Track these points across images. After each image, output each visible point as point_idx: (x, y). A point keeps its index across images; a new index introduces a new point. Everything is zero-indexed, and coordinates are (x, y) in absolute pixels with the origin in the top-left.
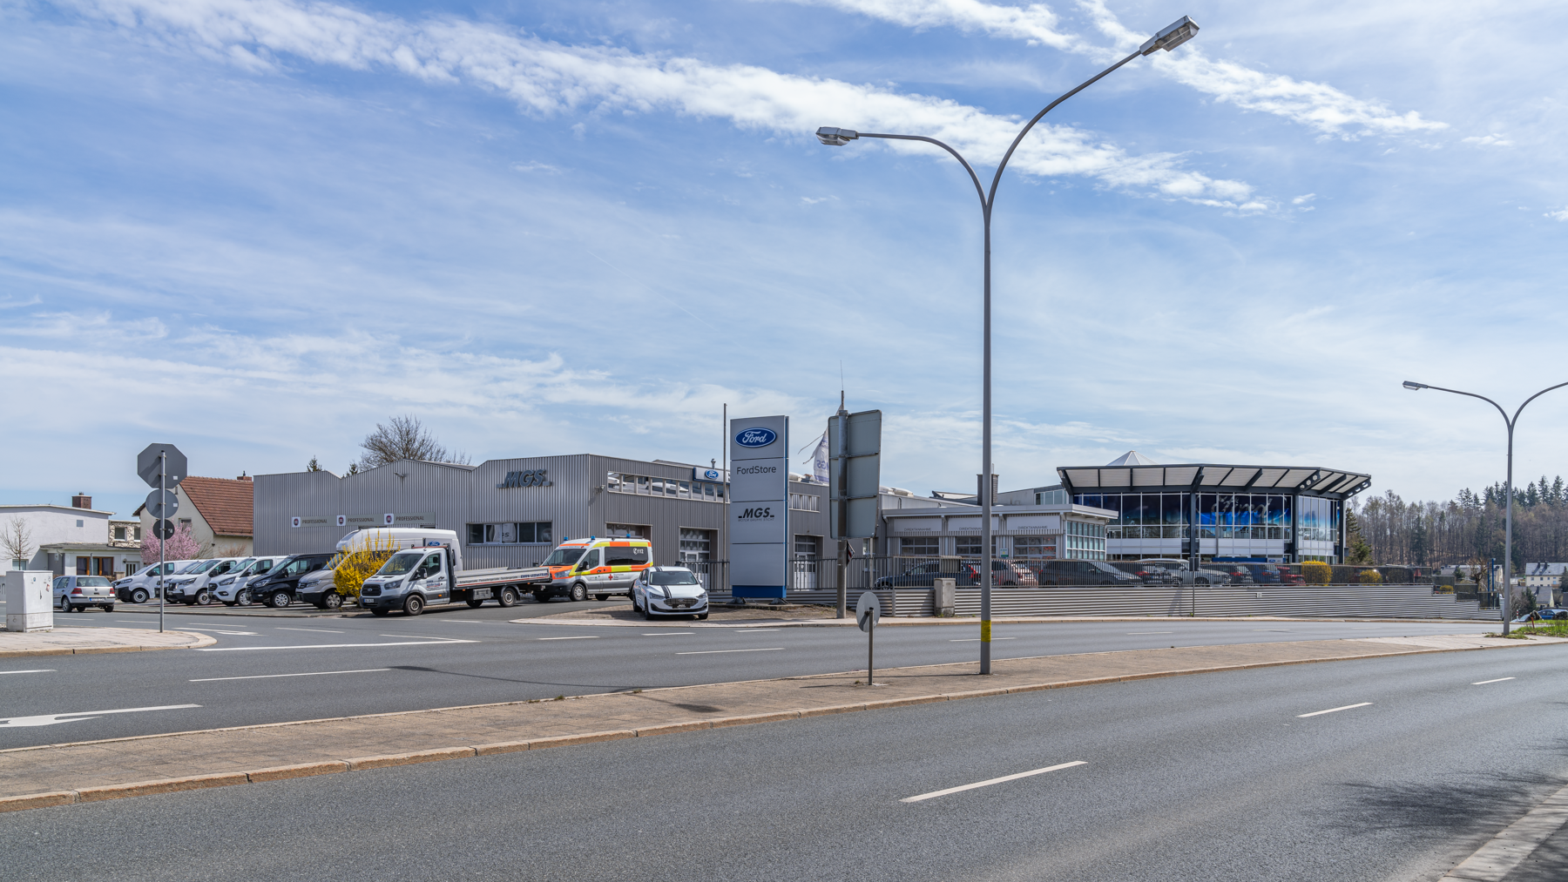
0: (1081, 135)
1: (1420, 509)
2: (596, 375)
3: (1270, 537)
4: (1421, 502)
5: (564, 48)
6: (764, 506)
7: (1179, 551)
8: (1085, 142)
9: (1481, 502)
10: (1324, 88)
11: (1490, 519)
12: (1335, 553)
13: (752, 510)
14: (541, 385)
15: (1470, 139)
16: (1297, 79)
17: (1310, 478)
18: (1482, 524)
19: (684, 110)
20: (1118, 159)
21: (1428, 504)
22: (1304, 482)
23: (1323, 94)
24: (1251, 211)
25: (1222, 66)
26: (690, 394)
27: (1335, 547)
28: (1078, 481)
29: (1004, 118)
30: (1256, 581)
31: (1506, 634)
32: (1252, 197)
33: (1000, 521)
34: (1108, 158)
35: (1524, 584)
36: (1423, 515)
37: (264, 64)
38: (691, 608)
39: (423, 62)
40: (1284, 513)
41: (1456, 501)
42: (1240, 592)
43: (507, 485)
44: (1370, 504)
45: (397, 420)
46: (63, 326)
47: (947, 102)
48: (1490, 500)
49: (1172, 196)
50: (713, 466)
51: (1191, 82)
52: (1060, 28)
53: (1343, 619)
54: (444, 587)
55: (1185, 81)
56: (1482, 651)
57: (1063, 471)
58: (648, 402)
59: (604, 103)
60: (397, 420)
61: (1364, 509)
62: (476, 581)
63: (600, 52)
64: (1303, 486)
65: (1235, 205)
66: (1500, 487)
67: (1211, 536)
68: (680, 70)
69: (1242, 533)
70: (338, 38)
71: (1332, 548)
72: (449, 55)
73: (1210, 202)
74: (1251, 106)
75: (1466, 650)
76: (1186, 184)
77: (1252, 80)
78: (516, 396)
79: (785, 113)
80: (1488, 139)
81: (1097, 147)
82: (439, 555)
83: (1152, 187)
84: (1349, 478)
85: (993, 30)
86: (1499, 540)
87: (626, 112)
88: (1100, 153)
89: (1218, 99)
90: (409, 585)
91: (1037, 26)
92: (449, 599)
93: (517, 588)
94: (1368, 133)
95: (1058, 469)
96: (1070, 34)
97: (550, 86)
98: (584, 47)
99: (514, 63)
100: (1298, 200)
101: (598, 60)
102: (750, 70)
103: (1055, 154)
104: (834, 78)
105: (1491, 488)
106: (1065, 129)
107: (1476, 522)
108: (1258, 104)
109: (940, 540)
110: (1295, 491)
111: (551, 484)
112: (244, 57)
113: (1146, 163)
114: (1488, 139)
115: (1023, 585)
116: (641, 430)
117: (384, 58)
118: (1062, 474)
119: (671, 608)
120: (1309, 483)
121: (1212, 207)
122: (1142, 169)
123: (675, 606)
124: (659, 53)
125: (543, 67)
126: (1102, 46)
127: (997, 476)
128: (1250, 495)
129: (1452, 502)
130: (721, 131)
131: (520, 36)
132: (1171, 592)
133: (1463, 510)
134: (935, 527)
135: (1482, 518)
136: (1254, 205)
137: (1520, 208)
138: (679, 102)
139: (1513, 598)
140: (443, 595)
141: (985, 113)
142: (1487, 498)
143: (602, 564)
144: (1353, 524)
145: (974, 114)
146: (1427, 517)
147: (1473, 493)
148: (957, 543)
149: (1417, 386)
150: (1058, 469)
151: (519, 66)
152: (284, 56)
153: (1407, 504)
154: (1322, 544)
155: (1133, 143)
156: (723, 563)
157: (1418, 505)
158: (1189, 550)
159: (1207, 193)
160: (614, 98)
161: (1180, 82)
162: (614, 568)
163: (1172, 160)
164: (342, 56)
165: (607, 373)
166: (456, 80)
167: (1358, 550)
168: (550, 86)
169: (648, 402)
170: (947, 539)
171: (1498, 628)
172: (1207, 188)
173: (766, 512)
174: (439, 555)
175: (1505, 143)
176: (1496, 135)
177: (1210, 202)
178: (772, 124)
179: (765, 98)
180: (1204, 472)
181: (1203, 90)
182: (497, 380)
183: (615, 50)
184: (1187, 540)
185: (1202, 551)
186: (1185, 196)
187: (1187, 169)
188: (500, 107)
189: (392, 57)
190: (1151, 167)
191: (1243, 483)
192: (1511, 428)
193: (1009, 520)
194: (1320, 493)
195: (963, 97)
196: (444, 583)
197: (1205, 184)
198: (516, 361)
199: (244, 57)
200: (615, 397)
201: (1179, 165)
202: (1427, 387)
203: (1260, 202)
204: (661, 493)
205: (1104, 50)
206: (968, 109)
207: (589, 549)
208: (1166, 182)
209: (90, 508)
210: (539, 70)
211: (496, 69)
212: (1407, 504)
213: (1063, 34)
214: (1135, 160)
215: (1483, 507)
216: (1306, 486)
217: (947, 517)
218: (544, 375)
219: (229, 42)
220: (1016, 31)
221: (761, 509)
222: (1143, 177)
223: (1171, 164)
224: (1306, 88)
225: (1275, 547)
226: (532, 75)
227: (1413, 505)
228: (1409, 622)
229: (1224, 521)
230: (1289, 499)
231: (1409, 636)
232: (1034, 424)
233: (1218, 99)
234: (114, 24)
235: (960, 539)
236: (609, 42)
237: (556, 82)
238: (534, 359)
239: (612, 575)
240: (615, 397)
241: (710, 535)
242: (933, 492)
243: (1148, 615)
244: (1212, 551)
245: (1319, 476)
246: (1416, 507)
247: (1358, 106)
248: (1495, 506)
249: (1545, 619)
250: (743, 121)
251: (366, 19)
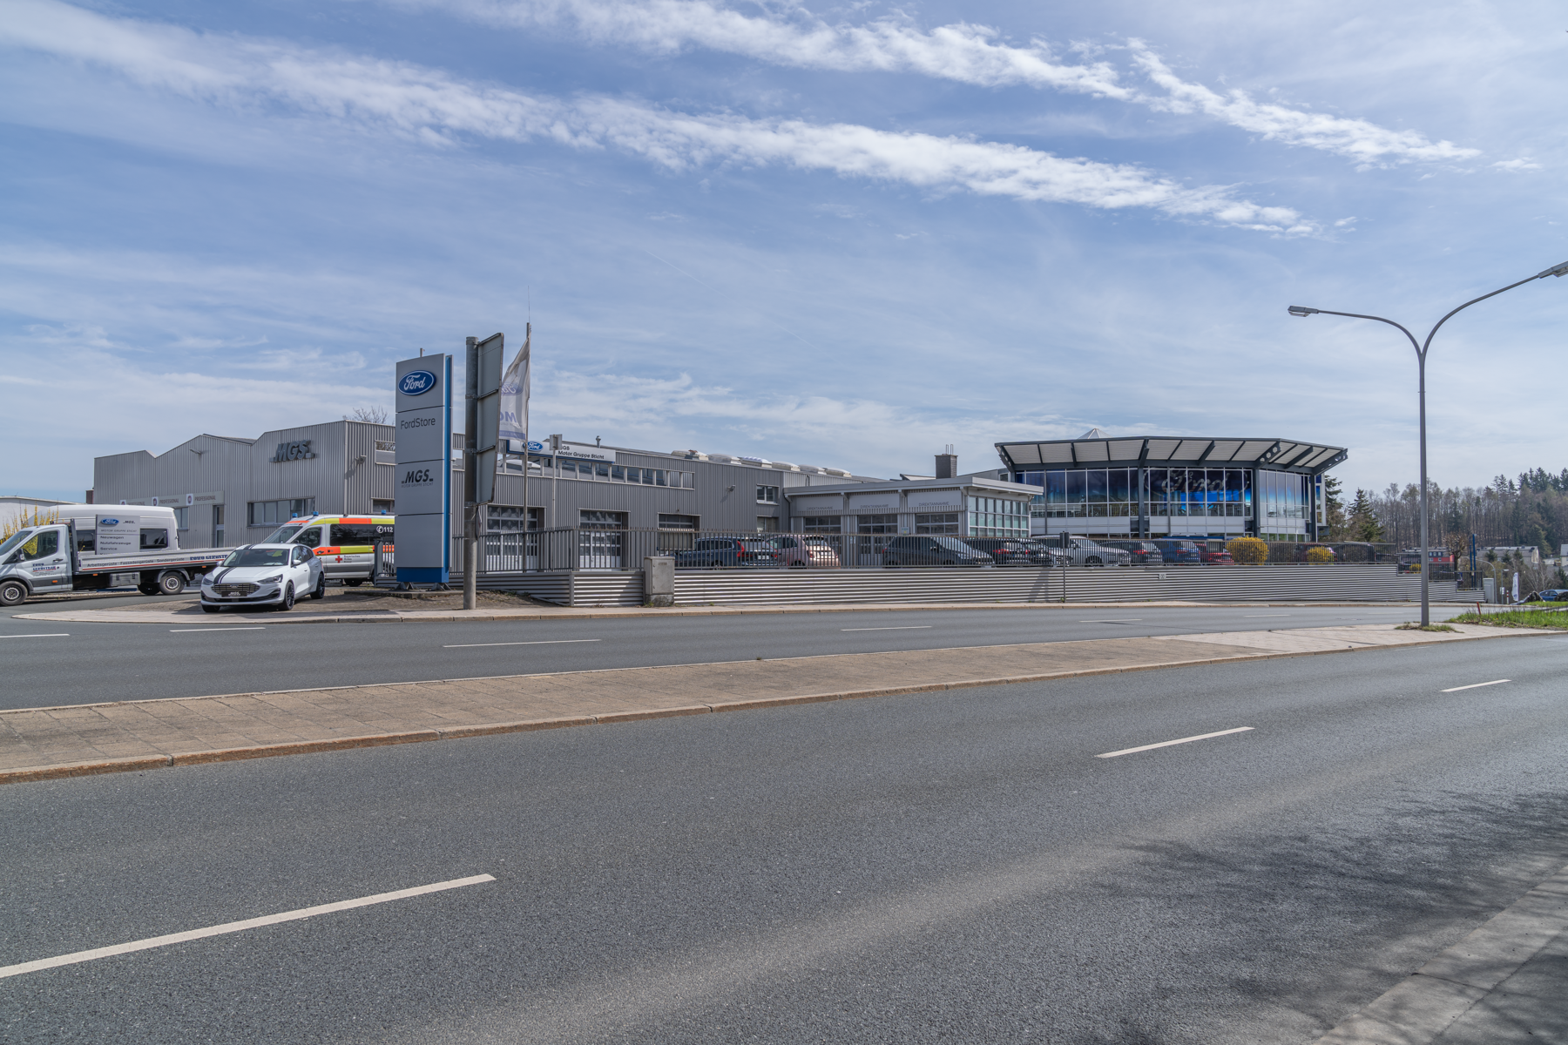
0: (1142, 173)
1: (1457, 495)
2: (720, 391)
3: (1229, 514)
4: (1457, 488)
5: (691, 117)
6: (423, 467)
7: (1127, 530)
8: (1146, 179)
9: (1516, 487)
10: (1360, 123)
11: (1525, 504)
12: (1307, 531)
13: (413, 473)
14: (672, 401)
15: (1500, 163)
16: (1337, 117)
17: (1270, 450)
18: (1517, 508)
19: (794, 164)
20: (1175, 192)
21: (1465, 490)
22: (1264, 455)
23: (1360, 129)
24: (1297, 233)
25: (1266, 108)
26: (800, 405)
27: (1307, 525)
28: (1020, 457)
29: (1072, 160)
30: (1167, 560)
31: (1425, 625)
32: (1298, 221)
33: (901, 498)
34: (1166, 192)
35: (1560, 564)
36: (1459, 501)
37: (446, 141)
38: (249, 596)
39: (575, 134)
40: (1243, 489)
41: (1491, 487)
42: (1139, 572)
43: (279, 459)
44: (1408, 491)
45: (361, 411)
46: (283, 361)
47: (1022, 149)
48: (1525, 485)
49: (1225, 222)
50: (598, 444)
51: (1240, 123)
52: (1121, 83)
53: (1267, 604)
54: (63, 570)
55: (1234, 124)
56: (1352, 654)
57: (1002, 447)
58: (765, 413)
59: (727, 161)
60: (361, 411)
61: (1403, 495)
62: (183, 559)
63: (722, 120)
64: (1263, 460)
65: (1281, 229)
66: (1534, 473)
67: (1163, 513)
68: (789, 131)
69: (1196, 510)
70: (507, 118)
71: (1304, 525)
72: (597, 127)
73: (1257, 227)
74: (1296, 142)
75: (1315, 653)
76: (1237, 212)
77: (1296, 120)
78: (651, 410)
79: (880, 164)
80: (1516, 163)
81: (1156, 183)
82: (56, 533)
83: (1208, 215)
84: (1316, 451)
85: (1061, 87)
86: (1535, 522)
87: (744, 168)
88: (1158, 188)
89: (1266, 137)
90: (3, 568)
91: (1098, 81)
92: (71, 586)
93: (185, 573)
94: (1405, 161)
95: (996, 445)
96: (1130, 88)
97: (681, 149)
98: (709, 116)
99: (651, 131)
100: (1341, 223)
101: (719, 126)
102: (850, 128)
103: (1119, 190)
104: (923, 132)
105: (1525, 474)
106: (1128, 168)
107: (1512, 506)
108: (1303, 140)
110: (1256, 464)
111: (314, 456)
112: (430, 136)
113: (1200, 195)
114: (1516, 163)
115: (814, 565)
116: (758, 437)
117: (544, 132)
118: (1000, 449)
119: (220, 597)
120: (1269, 455)
121: (1260, 231)
122: (1197, 200)
123: (224, 594)
124: (772, 118)
125: (675, 133)
126: (1159, 96)
127: (956, 457)
128: (1205, 470)
129: (1487, 488)
130: (826, 181)
131: (655, 109)
132: (1035, 573)
133: (1498, 495)
134: (836, 506)
135: (1517, 503)
136: (1300, 228)
137: (1550, 223)
138: (790, 159)
139: (1546, 578)
140: (61, 581)
141: (1056, 157)
142: (1522, 484)
143: (325, 543)
144: (1364, 506)
145: (1045, 158)
146: (1463, 502)
147: (1508, 479)
148: (859, 522)
149: (1306, 311)
150: (996, 445)
151: (655, 134)
152: (463, 134)
153: (1444, 489)
154: (1291, 521)
155: (1189, 178)
157: (1454, 491)
158: (1139, 529)
159: (1257, 219)
160: (735, 156)
161: (1230, 124)
162: (343, 548)
163: (1225, 191)
164: (509, 132)
165: (729, 389)
166: (602, 147)
167: (1365, 530)
168: (681, 149)
169: (765, 413)
170: (906, 516)
171: (1413, 613)
172: (1257, 215)
174: (56, 533)
175: (1534, 166)
176: (1526, 158)
177: (1257, 227)
178: (869, 174)
179: (864, 152)
180: (1149, 446)
181: (1252, 130)
182: (635, 397)
183: (735, 117)
184: (1136, 518)
185: (1152, 530)
186: (1237, 222)
187: (1238, 198)
188: (638, 168)
189: (550, 131)
190: (1205, 198)
191: (1196, 458)
192: (1422, 357)
193: (911, 497)
194: (1286, 467)
195: (1035, 144)
196: (63, 566)
197: (1255, 211)
198: (652, 381)
199: (430, 136)
200: (735, 409)
201: (1231, 195)
202: (1318, 312)
203: (1306, 225)
204: (573, 474)
205: (1163, 99)
206: (1040, 154)
207: (306, 527)
208: (1219, 211)
210: (671, 136)
211: (635, 137)
212: (1444, 489)
213: (1124, 87)
214: (1191, 192)
215: (1518, 492)
216: (1266, 459)
217: (848, 495)
218: (676, 392)
219: (418, 125)
220: (1082, 86)
221: (421, 472)
222: (1199, 207)
223: (1224, 194)
224: (1344, 125)
225: (1235, 524)
226: (665, 140)
227: (1450, 491)
228: (1358, 606)
229: (1178, 497)
230: (1248, 473)
231: (1274, 630)
232: (1105, 425)
233: (1266, 137)
234: (328, 115)
236: (728, 111)
237: (686, 146)
238: (667, 379)
239: (342, 556)
240: (735, 409)
241: (622, 517)
242: (901, 475)
243: (997, 601)
244: (1164, 530)
245: (1279, 448)
246: (1452, 492)
247: (1394, 137)
248: (1530, 491)
249: (1546, 600)
250: (844, 172)
251: (529, 101)
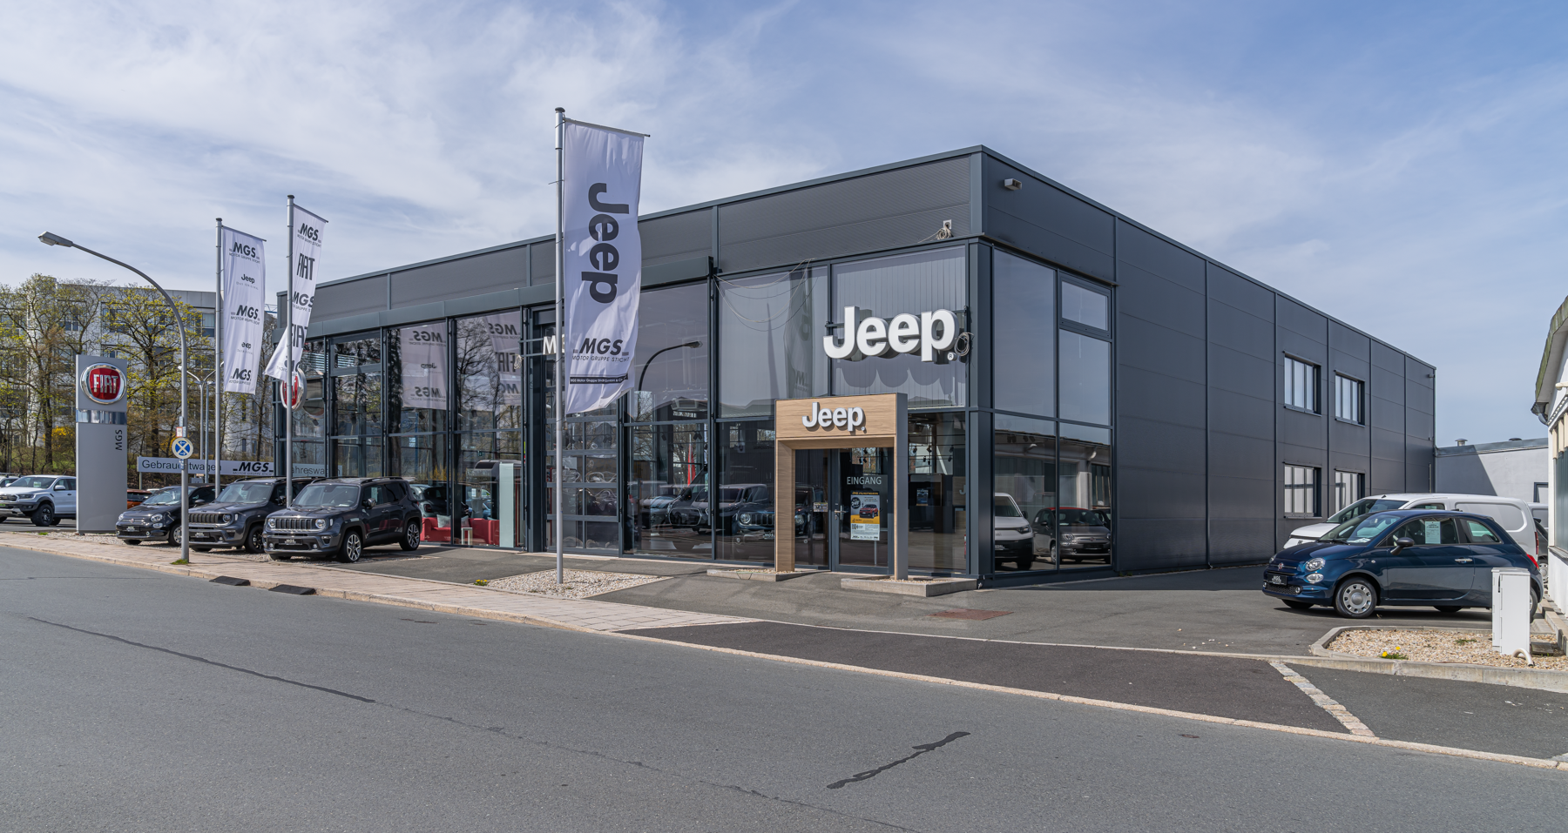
173: (264, 466)
221: (608, 341)
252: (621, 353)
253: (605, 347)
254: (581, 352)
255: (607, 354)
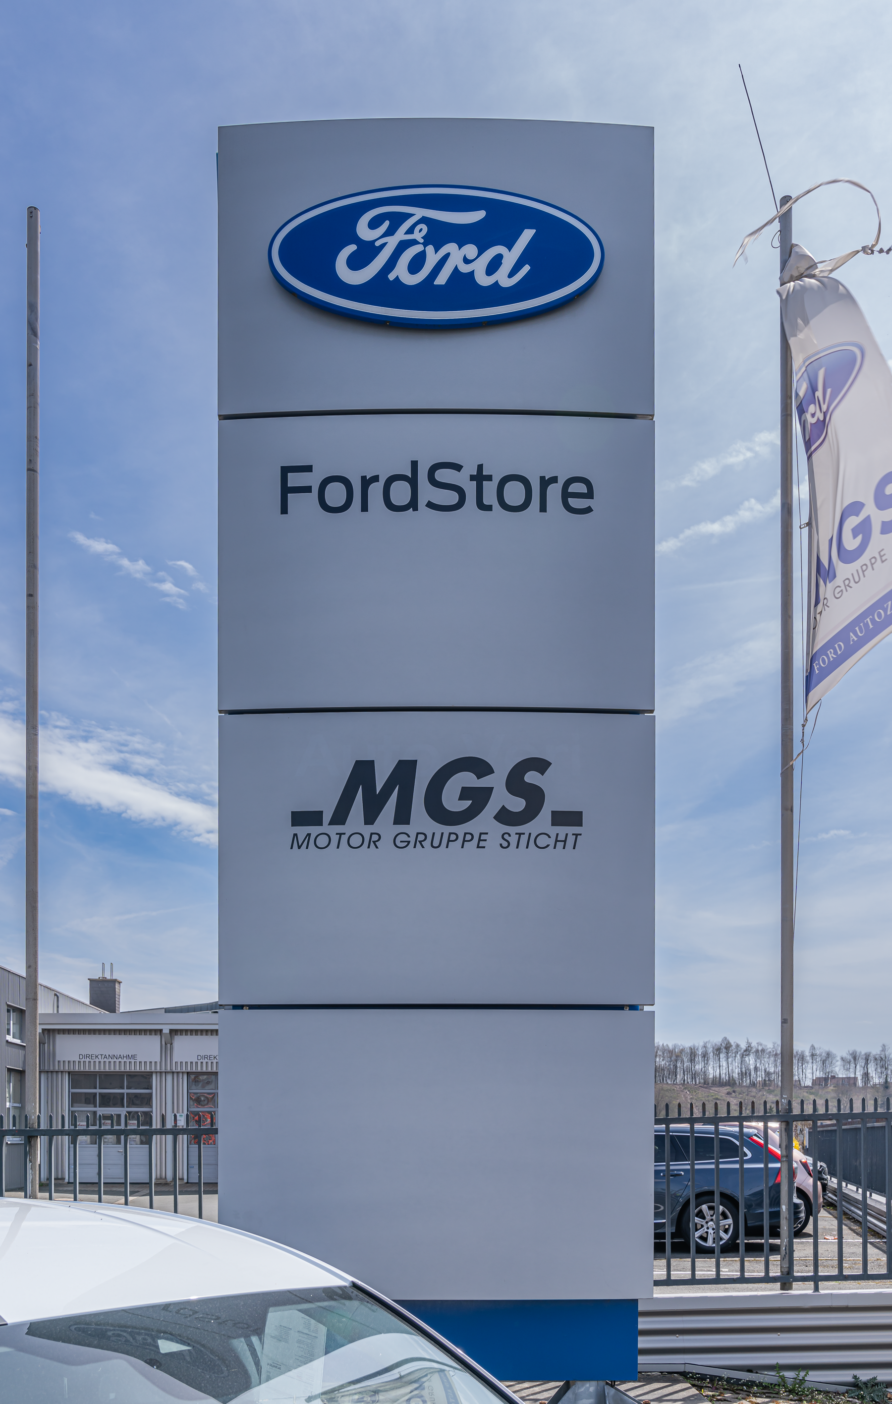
109: (155, 1080)
148: (74, 1084)
156: (30, 1137)
170: (169, 1077)
193: (179, 1042)
209: (203, 1194)
221: (481, 767)
235: (78, 1078)
252: (545, 815)
253: (466, 793)
254: (340, 817)
255: (485, 821)
